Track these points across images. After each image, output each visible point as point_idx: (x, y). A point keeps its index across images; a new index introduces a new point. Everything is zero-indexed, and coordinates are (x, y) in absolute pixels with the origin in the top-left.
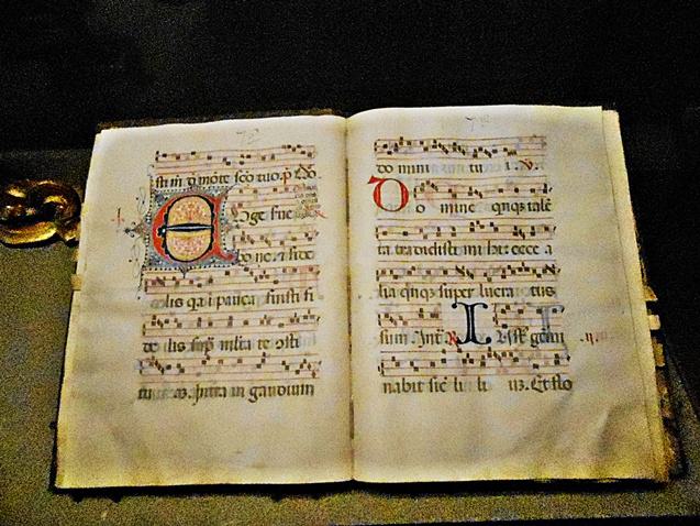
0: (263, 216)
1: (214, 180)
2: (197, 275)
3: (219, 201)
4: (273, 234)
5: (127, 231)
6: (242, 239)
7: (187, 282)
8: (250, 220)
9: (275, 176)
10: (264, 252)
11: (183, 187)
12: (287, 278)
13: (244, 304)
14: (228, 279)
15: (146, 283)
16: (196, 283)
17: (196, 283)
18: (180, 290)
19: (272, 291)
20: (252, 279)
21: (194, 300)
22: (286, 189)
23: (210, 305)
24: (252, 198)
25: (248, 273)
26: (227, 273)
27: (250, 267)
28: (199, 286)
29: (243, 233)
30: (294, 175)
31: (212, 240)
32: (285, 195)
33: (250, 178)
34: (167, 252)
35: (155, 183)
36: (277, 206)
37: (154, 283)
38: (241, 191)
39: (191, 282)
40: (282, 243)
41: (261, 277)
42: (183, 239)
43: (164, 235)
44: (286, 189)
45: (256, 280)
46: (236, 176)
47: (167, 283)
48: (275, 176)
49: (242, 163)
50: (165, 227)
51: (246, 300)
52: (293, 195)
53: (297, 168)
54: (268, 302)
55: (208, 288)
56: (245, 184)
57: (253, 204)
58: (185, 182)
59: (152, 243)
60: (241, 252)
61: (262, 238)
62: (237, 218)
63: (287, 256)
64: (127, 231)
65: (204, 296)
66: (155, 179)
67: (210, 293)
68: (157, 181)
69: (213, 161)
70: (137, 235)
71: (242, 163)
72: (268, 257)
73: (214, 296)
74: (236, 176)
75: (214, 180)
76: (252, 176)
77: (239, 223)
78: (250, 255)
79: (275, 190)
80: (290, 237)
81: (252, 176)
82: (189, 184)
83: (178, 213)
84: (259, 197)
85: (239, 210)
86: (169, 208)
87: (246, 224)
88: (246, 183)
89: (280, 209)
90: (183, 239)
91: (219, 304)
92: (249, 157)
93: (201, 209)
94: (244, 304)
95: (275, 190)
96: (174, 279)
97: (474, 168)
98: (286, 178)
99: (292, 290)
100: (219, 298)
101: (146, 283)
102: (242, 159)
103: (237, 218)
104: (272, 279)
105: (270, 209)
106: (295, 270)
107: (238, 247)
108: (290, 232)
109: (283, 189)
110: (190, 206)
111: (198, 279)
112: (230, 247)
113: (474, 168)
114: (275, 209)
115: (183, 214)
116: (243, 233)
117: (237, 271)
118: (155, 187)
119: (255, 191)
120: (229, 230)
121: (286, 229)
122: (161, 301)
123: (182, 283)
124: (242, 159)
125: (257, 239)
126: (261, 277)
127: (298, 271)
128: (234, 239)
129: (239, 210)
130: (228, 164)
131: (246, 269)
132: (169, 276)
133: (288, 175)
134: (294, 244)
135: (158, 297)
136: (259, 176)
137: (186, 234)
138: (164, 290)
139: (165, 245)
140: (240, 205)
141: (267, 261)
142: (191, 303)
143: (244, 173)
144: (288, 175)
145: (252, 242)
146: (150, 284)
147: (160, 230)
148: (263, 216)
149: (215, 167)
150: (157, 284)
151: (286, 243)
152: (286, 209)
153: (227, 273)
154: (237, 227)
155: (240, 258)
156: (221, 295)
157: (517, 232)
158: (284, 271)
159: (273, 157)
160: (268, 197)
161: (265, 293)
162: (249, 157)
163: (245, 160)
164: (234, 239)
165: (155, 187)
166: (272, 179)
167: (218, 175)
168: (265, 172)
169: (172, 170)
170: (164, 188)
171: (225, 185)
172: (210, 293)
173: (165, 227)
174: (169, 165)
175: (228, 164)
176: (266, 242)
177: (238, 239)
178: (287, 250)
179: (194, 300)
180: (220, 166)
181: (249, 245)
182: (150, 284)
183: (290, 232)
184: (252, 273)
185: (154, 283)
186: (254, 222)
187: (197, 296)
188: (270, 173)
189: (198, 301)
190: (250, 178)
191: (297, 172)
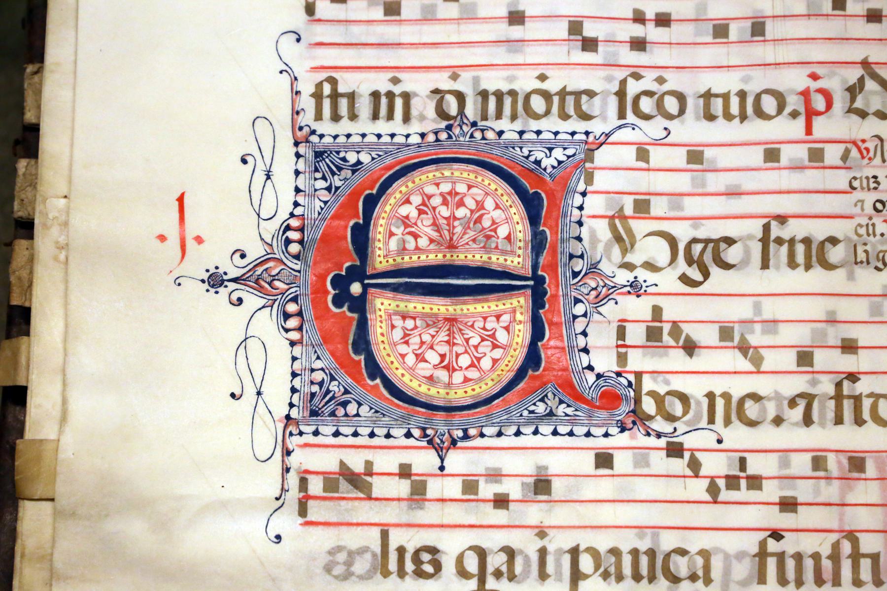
0: (732, 254)
1: (538, 105)
2: (491, 460)
3: (564, 185)
4: (772, 324)
5: (215, 281)
6: (654, 334)
7: (453, 488)
8: (682, 266)
9: (769, 104)
10: (738, 388)
11: (415, 127)
12: (831, 491)
13: (675, 580)
14: (604, 487)
15: (303, 483)
16: (487, 490)
17: (487, 490)
18: (430, 514)
19: (776, 535)
20: (698, 488)
21: (482, 554)
22: (816, 156)
23: (543, 575)
24: (682, 182)
25: (679, 465)
26: (604, 460)
27: (689, 441)
28: (501, 502)
29: (657, 311)
30: (840, 102)
31: (537, 333)
32: (812, 178)
33: (671, 105)
34: (374, 370)
35: (307, 103)
36: (782, 219)
37: (331, 484)
38: (642, 154)
39: (470, 486)
40: (805, 358)
41: (732, 482)
42: (432, 320)
43: (360, 305)
44: (816, 156)
45: (713, 490)
46: (621, 94)
47: (380, 487)
48: (769, 104)
49: (639, 44)
50: (358, 273)
51: (681, 566)
52: (841, 179)
53: (853, 75)
54: (762, 579)
55: (534, 514)
56: (654, 129)
57: (693, 207)
58: (424, 107)
59: (312, 333)
60: (648, 384)
61: (726, 333)
62: (634, 258)
63: (825, 409)
64: (215, 281)
65: (514, 538)
66: (307, 87)
67: (542, 534)
68: (318, 96)
69: (530, 30)
70: (253, 301)
71: (639, 44)
72: (752, 410)
73: (560, 542)
74: (621, 94)
75: (538, 105)
76: (681, 98)
77: (643, 275)
78: (684, 398)
79: (772, 155)
80: (834, 335)
81: (681, 98)
82: (442, 114)
83: (405, 221)
84: (716, 182)
85: (640, 227)
86: (371, 203)
87: (668, 280)
88: (660, 122)
89: (796, 229)
90: (432, 320)
91: (577, 576)
92: (663, 20)
93: (492, 214)
94: (675, 580)
95: (772, 155)
96: (405, 472)
97: (717, 105)
98: (811, 114)
99: (851, 536)
100: (575, 552)
101: (303, 483)
102: (637, 31)
103: (634, 258)
104: (771, 491)
105: (755, 227)
106: (857, 463)
107: (637, 361)
108: (832, 321)
109: (801, 152)
110: (453, 198)
111: (495, 476)
112: (604, 362)
113: (717, 105)
114: (776, 231)
115: (425, 228)
116: (657, 311)
117: (641, 455)
118: (307, 118)
119: (695, 156)
120: (600, 300)
121: (816, 309)
122: (741, 556)
123: (434, 488)
124: (637, 31)
125: (707, 335)
126: (732, 482)
127: (871, 470)
128: (621, 333)
129: (640, 227)
130: (590, 45)
131: (675, 450)
132: (387, 462)
133: (819, 103)
134: (848, 363)
135: (353, 539)
136: (708, 96)
137: (440, 306)
138: (365, 512)
139: (362, 343)
140: (642, 207)
141: (752, 424)
142: (472, 564)
143: (648, 83)
144: (819, 103)
145: (690, 348)
146: (316, 486)
147: (340, 283)
148: (732, 254)
149: (533, 55)
150: (344, 485)
151: (821, 359)
152: (819, 230)
153: (604, 460)
154: (635, 289)
155: (649, 406)
156: (585, 540)
157: (507, 365)
158: (818, 463)
159: (758, 29)
160: (748, 182)
161: (750, 543)
162: (663, 20)
163: (653, 33)
164: (621, 333)
165: (307, 118)
166: (760, 113)
167: (548, 86)
168: (721, 83)
169: (369, 57)
170: (345, 126)
171: (580, 126)
172: (542, 534)
173: (358, 273)
174: (358, 33)
175: (590, 45)
176: (744, 348)
177: (636, 334)
178: (827, 387)
179: (482, 554)
180: (559, 54)
181: (677, 359)
182: (316, 486)
183: (832, 321)
184: (695, 465)
185: (331, 484)
186: (695, 274)
187: (492, 541)
188: (753, 88)
189: (496, 561)
190: (671, 105)
191: (854, 90)
